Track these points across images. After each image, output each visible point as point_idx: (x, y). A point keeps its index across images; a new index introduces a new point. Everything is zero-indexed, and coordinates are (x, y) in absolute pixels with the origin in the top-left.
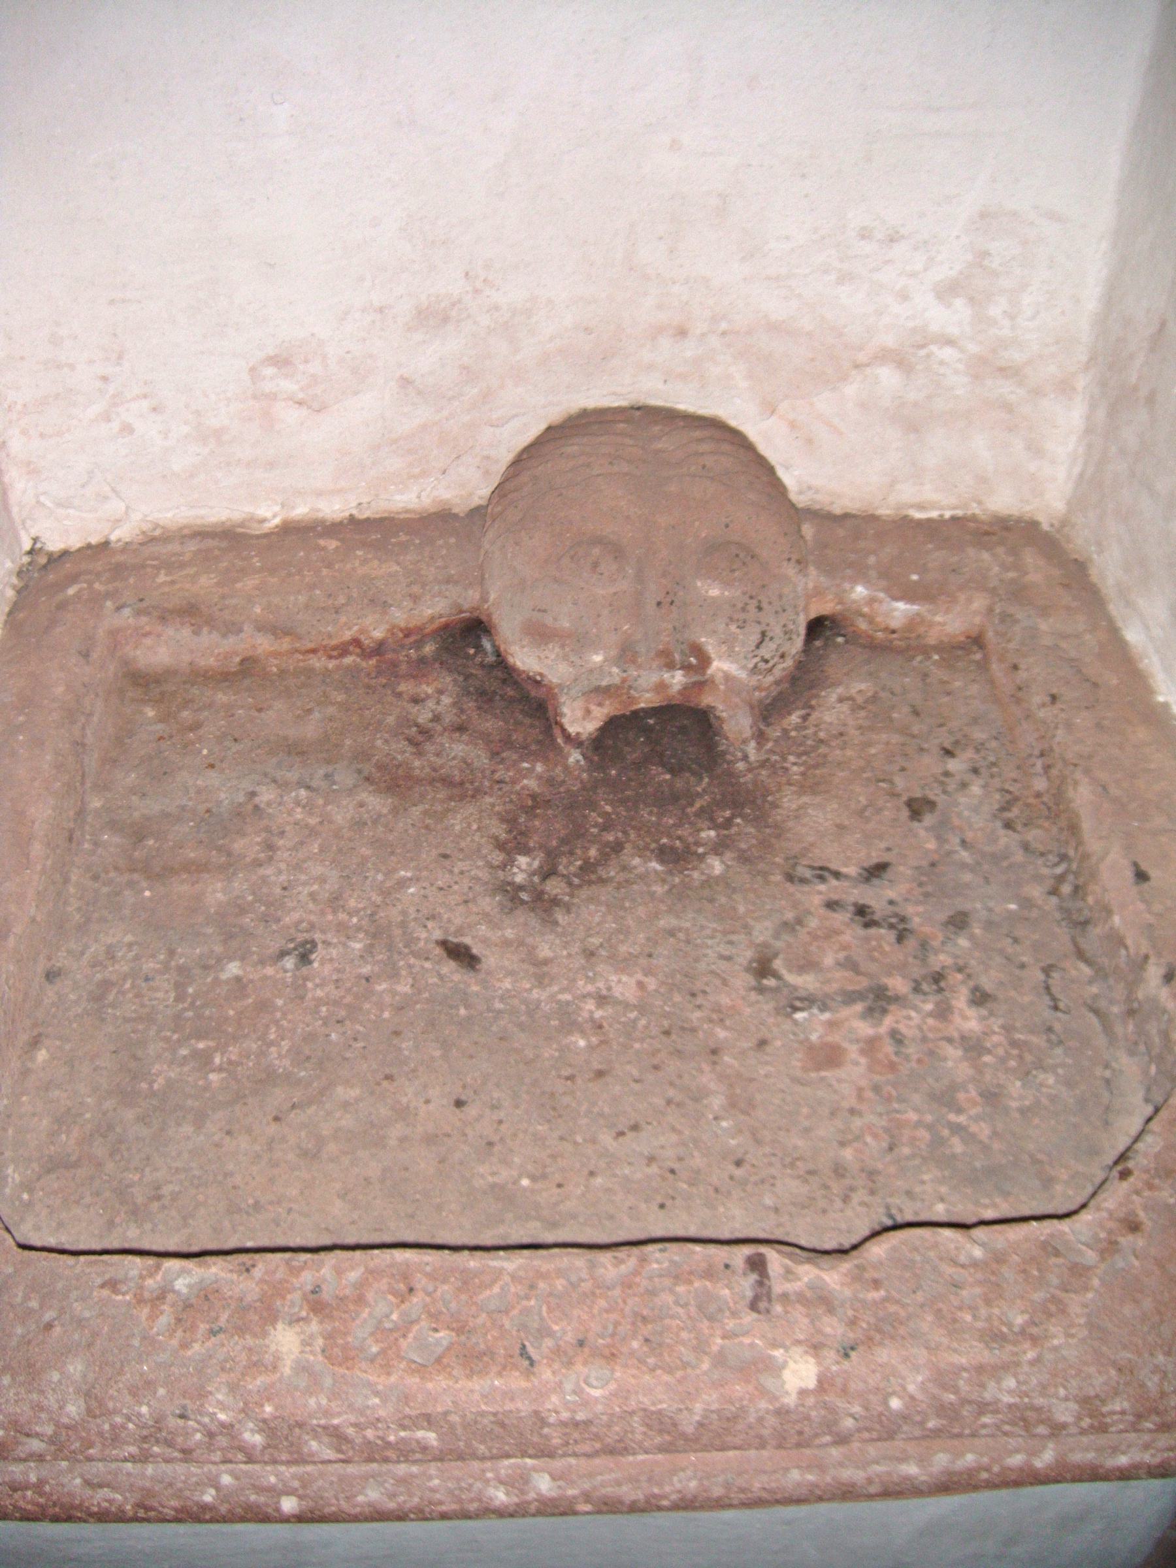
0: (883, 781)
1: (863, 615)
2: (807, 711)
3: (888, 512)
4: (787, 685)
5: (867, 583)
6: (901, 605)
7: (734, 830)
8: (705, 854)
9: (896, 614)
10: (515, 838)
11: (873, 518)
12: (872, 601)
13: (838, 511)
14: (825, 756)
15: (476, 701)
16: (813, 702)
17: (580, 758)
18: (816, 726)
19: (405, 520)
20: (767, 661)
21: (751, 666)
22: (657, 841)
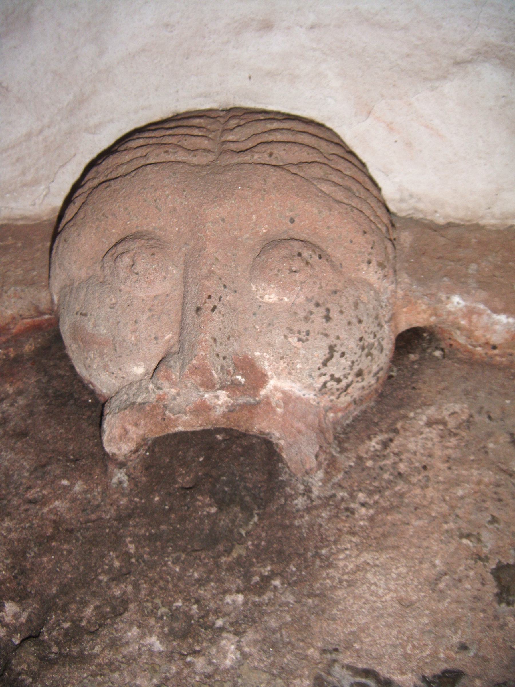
0: (468, 536)
1: (459, 328)
2: (391, 435)
3: (493, 222)
4: (373, 404)
5: (465, 293)
6: (503, 318)
7: (268, 595)
8: (222, 629)
9: (497, 327)
10: (15, 577)
11: (478, 228)
12: (470, 312)
13: (441, 221)
14: (402, 496)
15: (50, 404)
16: (399, 425)
17: (125, 478)
18: (396, 454)
19: (24, 226)
20: (339, 381)
21: (318, 385)
22: (169, 604)
